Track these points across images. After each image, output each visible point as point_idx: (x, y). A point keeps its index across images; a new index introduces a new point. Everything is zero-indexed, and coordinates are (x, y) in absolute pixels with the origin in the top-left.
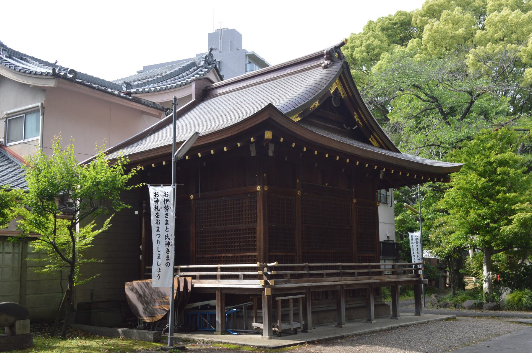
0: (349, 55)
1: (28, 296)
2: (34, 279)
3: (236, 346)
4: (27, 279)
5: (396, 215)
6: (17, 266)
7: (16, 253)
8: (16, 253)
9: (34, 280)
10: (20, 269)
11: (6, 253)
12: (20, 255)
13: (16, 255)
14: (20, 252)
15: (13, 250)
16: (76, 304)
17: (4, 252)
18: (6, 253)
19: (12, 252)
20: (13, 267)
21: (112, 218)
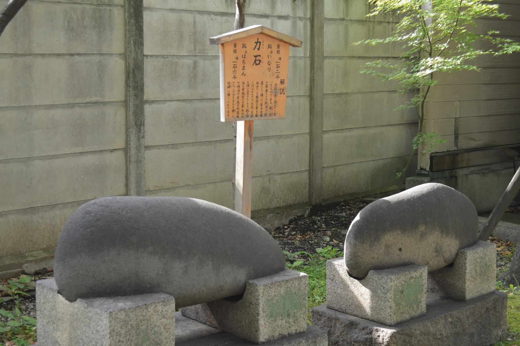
0: (346, 192)
1: (326, 136)
2: (338, 92)
3: (444, 153)
4: (325, 92)
5: (35, 329)
6: (302, 55)
7: (300, 18)
8: (300, 18)
9: (337, 94)
10: (308, 62)
11: (280, 17)
12: (309, 24)
13: (300, 24)
14: (309, 15)
15: (294, 9)
16: (428, 158)
17: (275, 15)
18: (280, 17)
19: (291, 14)
20: (294, 57)
21: (346, 240)
